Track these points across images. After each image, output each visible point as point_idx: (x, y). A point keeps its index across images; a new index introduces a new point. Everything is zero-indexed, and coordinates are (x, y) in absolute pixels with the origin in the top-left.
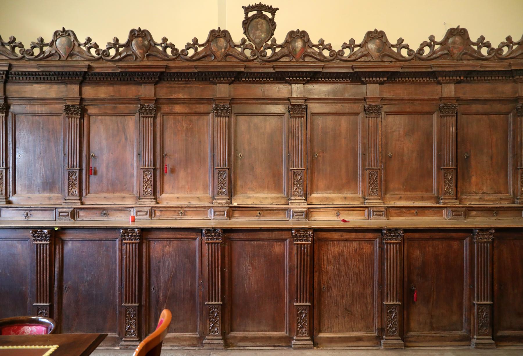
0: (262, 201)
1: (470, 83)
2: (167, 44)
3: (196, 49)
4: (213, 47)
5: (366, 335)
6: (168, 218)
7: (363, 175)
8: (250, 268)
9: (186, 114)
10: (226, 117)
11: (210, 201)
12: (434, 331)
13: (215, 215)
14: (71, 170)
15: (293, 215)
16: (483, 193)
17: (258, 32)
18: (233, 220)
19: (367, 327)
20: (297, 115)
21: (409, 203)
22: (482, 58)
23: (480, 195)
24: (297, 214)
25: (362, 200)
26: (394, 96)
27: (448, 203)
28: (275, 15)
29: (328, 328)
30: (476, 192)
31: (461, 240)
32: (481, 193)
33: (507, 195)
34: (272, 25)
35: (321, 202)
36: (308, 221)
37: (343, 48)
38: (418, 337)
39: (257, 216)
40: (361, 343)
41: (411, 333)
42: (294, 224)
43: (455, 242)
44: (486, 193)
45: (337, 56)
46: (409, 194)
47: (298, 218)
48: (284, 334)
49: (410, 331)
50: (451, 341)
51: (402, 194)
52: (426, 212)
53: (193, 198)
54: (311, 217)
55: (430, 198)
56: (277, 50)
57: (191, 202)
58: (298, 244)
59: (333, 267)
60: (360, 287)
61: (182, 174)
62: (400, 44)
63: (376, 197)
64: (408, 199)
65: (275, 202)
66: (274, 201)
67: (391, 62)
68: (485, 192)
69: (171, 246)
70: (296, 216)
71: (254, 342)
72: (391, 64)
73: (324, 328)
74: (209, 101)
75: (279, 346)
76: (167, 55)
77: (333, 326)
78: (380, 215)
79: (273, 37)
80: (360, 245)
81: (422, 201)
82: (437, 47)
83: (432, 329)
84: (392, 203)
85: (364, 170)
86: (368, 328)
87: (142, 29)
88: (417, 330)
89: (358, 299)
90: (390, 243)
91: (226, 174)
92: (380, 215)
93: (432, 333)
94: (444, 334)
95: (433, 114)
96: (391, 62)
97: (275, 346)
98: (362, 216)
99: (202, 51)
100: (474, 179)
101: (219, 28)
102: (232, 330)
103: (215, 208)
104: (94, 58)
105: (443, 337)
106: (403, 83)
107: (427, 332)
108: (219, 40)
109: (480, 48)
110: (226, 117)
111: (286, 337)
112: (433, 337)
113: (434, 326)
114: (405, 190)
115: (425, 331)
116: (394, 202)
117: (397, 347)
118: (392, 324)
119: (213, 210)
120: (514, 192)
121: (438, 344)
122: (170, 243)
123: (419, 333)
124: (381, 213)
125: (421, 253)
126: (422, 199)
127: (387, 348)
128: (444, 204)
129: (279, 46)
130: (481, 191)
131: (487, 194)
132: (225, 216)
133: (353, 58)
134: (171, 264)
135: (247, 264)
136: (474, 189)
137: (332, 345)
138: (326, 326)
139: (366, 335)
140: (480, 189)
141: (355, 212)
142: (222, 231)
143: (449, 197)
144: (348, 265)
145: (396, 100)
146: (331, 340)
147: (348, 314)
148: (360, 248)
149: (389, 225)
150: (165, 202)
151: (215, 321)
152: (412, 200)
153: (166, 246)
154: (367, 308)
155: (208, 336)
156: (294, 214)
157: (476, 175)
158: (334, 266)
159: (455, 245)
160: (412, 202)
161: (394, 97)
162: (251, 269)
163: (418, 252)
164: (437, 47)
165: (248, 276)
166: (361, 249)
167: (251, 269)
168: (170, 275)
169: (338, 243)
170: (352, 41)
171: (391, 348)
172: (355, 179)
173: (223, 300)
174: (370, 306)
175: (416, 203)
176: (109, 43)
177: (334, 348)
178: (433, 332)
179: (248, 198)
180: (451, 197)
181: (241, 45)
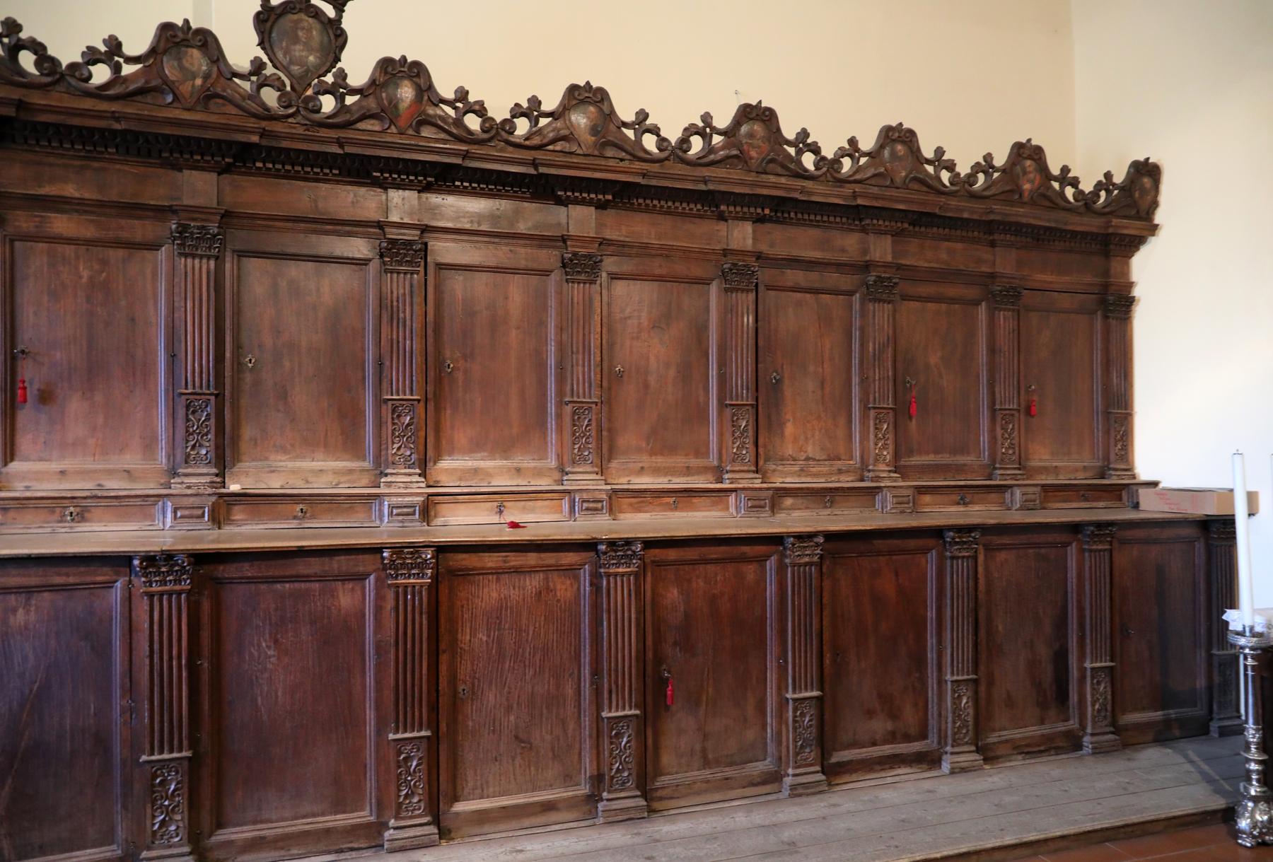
0: (309, 479)
1: (782, 223)
2: (19, 39)
3: (117, 68)
4: (170, 69)
5: (565, 794)
6: (30, 528)
7: (559, 416)
8: (271, 652)
9: (89, 243)
10: (209, 258)
11: (162, 481)
12: (710, 768)
13: (175, 517)
14: (397, 403)
15: (391, 514)
16: (808, 459)
17: (298, 47)
18: (228, 530)
19: (567, 776)
20: (402, 266)
21: (661, 480)
22: (803, 174)
23: (801, 462)
24: (399, 511)
25: (557, 475)
26: (627, 237)
27: (740, 481)
28: (343, 11)
29: (475, 788)
30: (794, 455)
31: (761, 560)
32: (803, 458)
33: (851, 462)
34: (337, 36)
35: (460, 479)
36: (427, 527)
37: (514, 116)
38: (677, 786)
39: (295, 518)
40: (553, 816)
41: (663, 778)
42: (391, 534)
43: (750, 567)
44: (812, 458)
45: (498, 131)
46: (660, 460)
47: (402, 521)
48: (365, 816)
49: (662, 775)
50: (744, 787)
51: (646, 460)
52: (695, 500)
53: (110, 473)
54: (435, 517)
55: (704, 470)
56: (350, 100)
57: (102, 482)
58: (397, 586)
59: (485, 638)
60: (549, 683)
61: (75, 406)
62: (803, 141)
63: (589, 469)
64: (657, 471)
65: (345, 482)
66: (343, 479)
67: (622, 160)
68: (810, 456)
69: (33, 609)
70: (398, 515)
71: (282, 848)
72: (621, 164)
73: (466, 791)
74: (161, 212)
75: (352, 849)
76: (22, 72)
77: (487, 783)
78: (596, 509)
79: (339, 65)
80: (548, 582)
81: (688, 476)
82: (717, 139)
83: (706, 763)
84: (624, 480)
85: (561, 404)
86: (568, 778)
87: (194, 25)
88: (675, 770)
89: (545, 711)
90: (616, 575)
91: (209, 409)
92: (596, 509)
93: (706, 773)
94: (729, 772)
95: (709, 284)
96: (622, 160)
97: (341, 851)
98: (556, 512)
99: (134, 76)
100: (789, 429)
101: (760, 102)
102: (220, 825)
103: (176, 500)
104: (649, 156)
105: (727, 779)
106: (647, 210)
107: (696, 773)
108: (186, 52)
109: (800, 152)
110: (398, 273)
111: (368, 825)
112: (708, 782)
113: (710, 756)
114: (652, 453)
115: (692, 771)
116: (629, 478)
117: (632, 816)
118: (621, 763)
119: (169, 504)
120: (862, 457)
121: (717, 797)
122: (28, 599)
123: (679, 776)
124: (599, 505)
125: (682, 594)
126: (688, 471)
127: (610, 819)
128: (731, 483)
129: (353, 91)
130: (802, 453)
131: (814, 460)
132: (206, 518)
133: (536, 141)
134: (31, 657)
135: (264, 644)
136: (789, 450)
137: (486, 828)
138: (471, 784)
139: (565, 794)
140: (801, 450)
141: (540, 503)
142: (192, 559)
143: (742, 468)
144: (520, 630)
145: (632, 247)
146: (482, 818)
147: (523, 748)
148: (548, 588)
149: (648, 532)
150: (20, 485)
151: (412, 780)
152: (666, 475)
153: (14, 611)
154: (565, 731)
155: (149, 849)
156: (392, 512)
157: (794, 418)
158: (489, 636)
159: (750, 571)
160: (666, 480)
161: (627, 239)
162: (274, 656)
163: (675, 591)
164: (717, 139)
165: (266, 675)
166: (551, 591)
167: (274, 656)
168: (27, 691)
169: (498, 580)
170: (535, 102)
171: (620, 818)
172: (542, 425)
173: (193, 745)
174: (571, 726)
175: (678, 480)
176: (517, 105)
177: (489, 837)
178: (708, 772)
179: (273, 471)
180: (745, 468)
181: (251, 74)
